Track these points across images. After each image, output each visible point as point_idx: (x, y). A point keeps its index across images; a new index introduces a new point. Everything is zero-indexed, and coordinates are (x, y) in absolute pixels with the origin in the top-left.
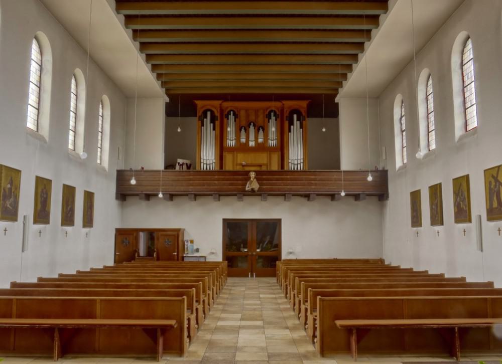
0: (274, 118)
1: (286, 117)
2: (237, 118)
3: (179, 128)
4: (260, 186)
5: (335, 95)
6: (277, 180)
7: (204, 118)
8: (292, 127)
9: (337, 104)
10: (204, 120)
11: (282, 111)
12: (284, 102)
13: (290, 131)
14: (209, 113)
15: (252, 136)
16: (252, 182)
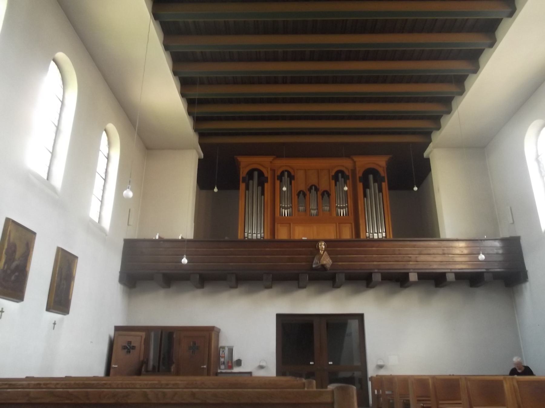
0: (343, 179)
1: (360, 177)
2: (294, 179)
3: (216, 188)
4: (333, 262)
5: (426, 145)
6: (358, 253)
7: (249, 180)
8: (368, 191)
9: (428, 160)
10: (248, 182)
11: (354, 171)
12: (356, 159)
13: (365, 195)
14: (256, 174)
15: (313, 206)
16: (322, 255)
